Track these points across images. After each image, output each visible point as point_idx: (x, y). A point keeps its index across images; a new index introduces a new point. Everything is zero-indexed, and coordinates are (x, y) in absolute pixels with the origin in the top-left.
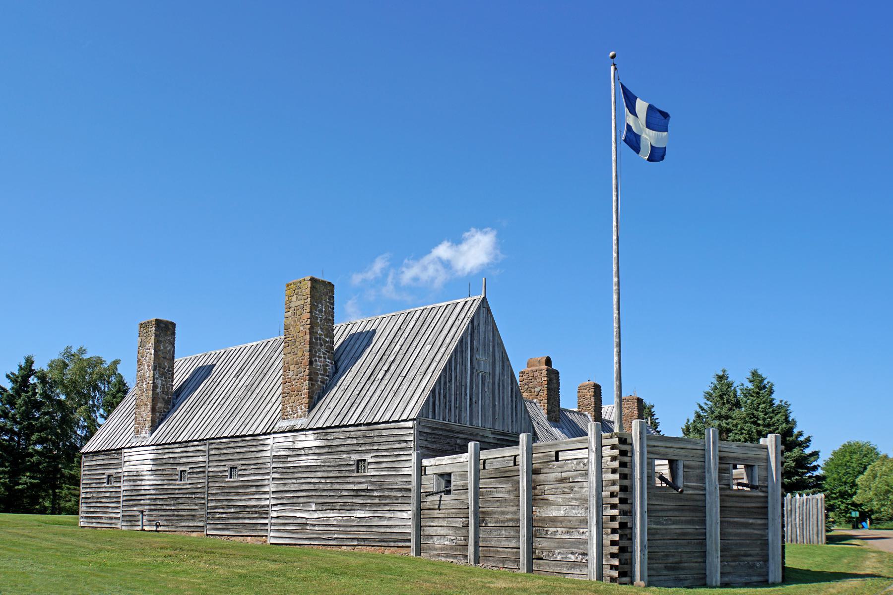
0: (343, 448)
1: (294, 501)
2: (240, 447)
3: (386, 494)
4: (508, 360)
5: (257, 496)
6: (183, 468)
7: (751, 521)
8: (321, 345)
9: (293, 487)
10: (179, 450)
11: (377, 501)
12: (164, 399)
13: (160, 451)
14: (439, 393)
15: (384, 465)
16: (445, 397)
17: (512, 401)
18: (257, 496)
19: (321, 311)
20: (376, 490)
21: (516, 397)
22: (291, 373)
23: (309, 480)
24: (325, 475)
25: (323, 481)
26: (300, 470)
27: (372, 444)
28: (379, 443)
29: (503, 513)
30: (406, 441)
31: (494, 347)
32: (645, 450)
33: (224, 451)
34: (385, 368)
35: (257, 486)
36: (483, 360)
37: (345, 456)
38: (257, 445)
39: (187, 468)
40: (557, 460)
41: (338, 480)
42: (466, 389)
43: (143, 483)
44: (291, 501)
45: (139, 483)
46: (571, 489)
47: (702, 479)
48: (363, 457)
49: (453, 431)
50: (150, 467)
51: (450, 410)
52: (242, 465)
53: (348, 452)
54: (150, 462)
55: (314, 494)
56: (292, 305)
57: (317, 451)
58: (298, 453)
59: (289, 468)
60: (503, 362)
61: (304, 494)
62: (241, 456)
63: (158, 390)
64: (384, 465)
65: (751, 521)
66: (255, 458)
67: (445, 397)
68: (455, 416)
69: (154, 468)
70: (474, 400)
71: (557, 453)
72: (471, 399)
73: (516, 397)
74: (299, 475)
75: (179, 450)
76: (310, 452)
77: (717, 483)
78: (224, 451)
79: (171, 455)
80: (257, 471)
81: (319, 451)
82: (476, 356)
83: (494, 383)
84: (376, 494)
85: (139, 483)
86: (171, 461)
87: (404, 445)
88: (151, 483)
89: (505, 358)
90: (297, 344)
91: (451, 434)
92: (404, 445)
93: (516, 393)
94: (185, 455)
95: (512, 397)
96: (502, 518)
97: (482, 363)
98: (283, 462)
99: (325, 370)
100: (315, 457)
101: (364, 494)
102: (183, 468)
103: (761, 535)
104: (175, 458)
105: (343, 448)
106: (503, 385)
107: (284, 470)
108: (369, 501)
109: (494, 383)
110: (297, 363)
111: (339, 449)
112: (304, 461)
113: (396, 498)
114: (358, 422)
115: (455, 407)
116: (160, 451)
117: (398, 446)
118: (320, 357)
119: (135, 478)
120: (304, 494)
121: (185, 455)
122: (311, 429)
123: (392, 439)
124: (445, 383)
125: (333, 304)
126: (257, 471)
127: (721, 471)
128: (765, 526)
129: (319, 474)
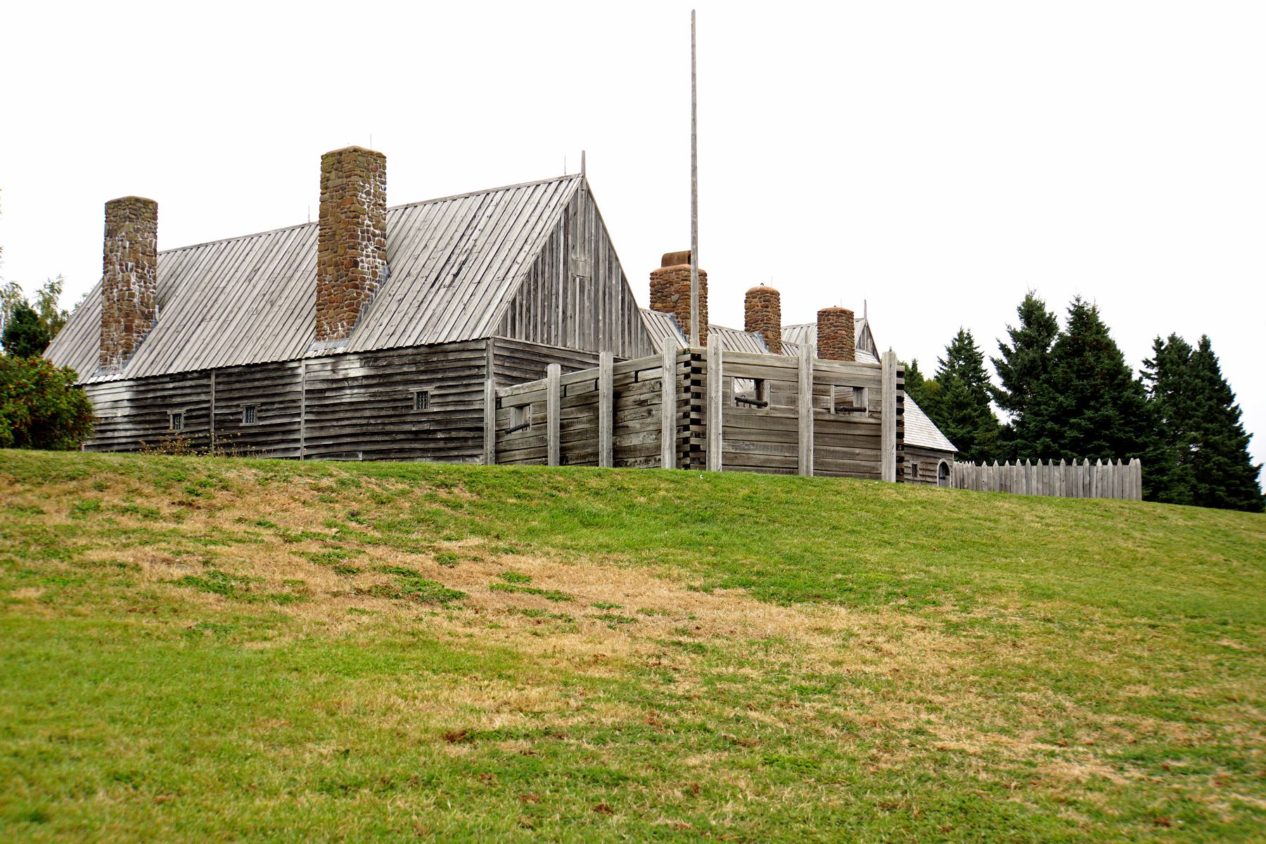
0: (399, 378)
1: (335, 449)
2: (258, 380)
3: (454, 434)
4: (617, 259)
5: (283, 446)
6: (177, 411)
7: (857, 451)
8: (369, 240)
9: (332, 432)
10: (171, 385)
11: (441, 444)
12: (143, 313)
13: (142, 388)
14: (521, 305)
15: (450, 399)
16: (528, 310)
17: (623, 315)
18: (283, 446)
19: (368, 193)
20: (440, 430)
21: (630, 310)
22: (328, 277)
23: (354, 422)
24: (375, 413)
25: (372, 421)
26: (343, 408)
27: (434, 371)
28: (444, 370)
29: (584, 446)
30: (478, 367)
31: (597, 242)
32: (721, 366)
33: (238, 386)
34: (454, 270)
35: (284, 433)
36: (582, 263)
37: (400, 388)
38: (282, 377)
39: (183, 411)
40: (636, 381)
41: (392, 420)
42: (557, 299)
43: (116, 434)
44: (330, 450)
45: (109, 434)
46: (649, 412)
47: (793, 401)
48: (425, 388)
49: (539, 355)
50: (127, 412)
51: (535, 327)
52: (263, 404)
53: (406, 382)
54: (126, 404)
55: (361, 439)
56: (330, 184)
57: (365, 382)
58: (339, 385)
59: (327, 406)
60: (610, 263)
61: (349, 440)
62: (260, 392)
63: (135, 300)
64: (450, 399)
65: (857, 451)
66: (280, 395)
67: (528, 310)
68: (542, 335)
69: (134, 412)
70: (569, 314)
71: (637, 372)
72: (564, 313)
73: (630, 310)
74: (341, 415)
75: (171, 385)
76: (355, 383)
77: (810, 405)
78: (238, 386)
79: (159, 394)
80: (283, 412)
81: (364, 383)
82: (572, 256)
83: (597, 291)
84: (440, 435)
85: (109, 434)
86: (159, 401)
87: (475, 371)
88: (128, 434)
89: (612, 258)
90: (337, 238)
91: (537, 359)
92: (475, 371)
93: (630, 304)
94: (179, 392)
95: (623, 309)
96: (582, 452)
97: (581, 264)
98: (319, 399)
99: (374, 274)
100: (362, 391)
101: (425, 436)
102: (177, 411)
103: (873, 468)
104: (164, 397)
105: (399, 378)
106: (610, 294)
107: (321, 410)
108: (432, 445)
109: (597, 291)
110: (336, 265)
111: (402, 437)
112: (348, 396)
113: (466, 439)
114: (418, 343)
115: (543, 324)
116: (142, 388)
117: (468, 373)
118: (368, 256)
119: (103, 428)
120: (349, 440)
121: (179, 392)
122: (356, 353)
123: (460, 364)
124: (529, 292)
125: (384, 183)
126: (283, 412)
127: (815, 392)
128: (878, 459)
129: (367, 413)
